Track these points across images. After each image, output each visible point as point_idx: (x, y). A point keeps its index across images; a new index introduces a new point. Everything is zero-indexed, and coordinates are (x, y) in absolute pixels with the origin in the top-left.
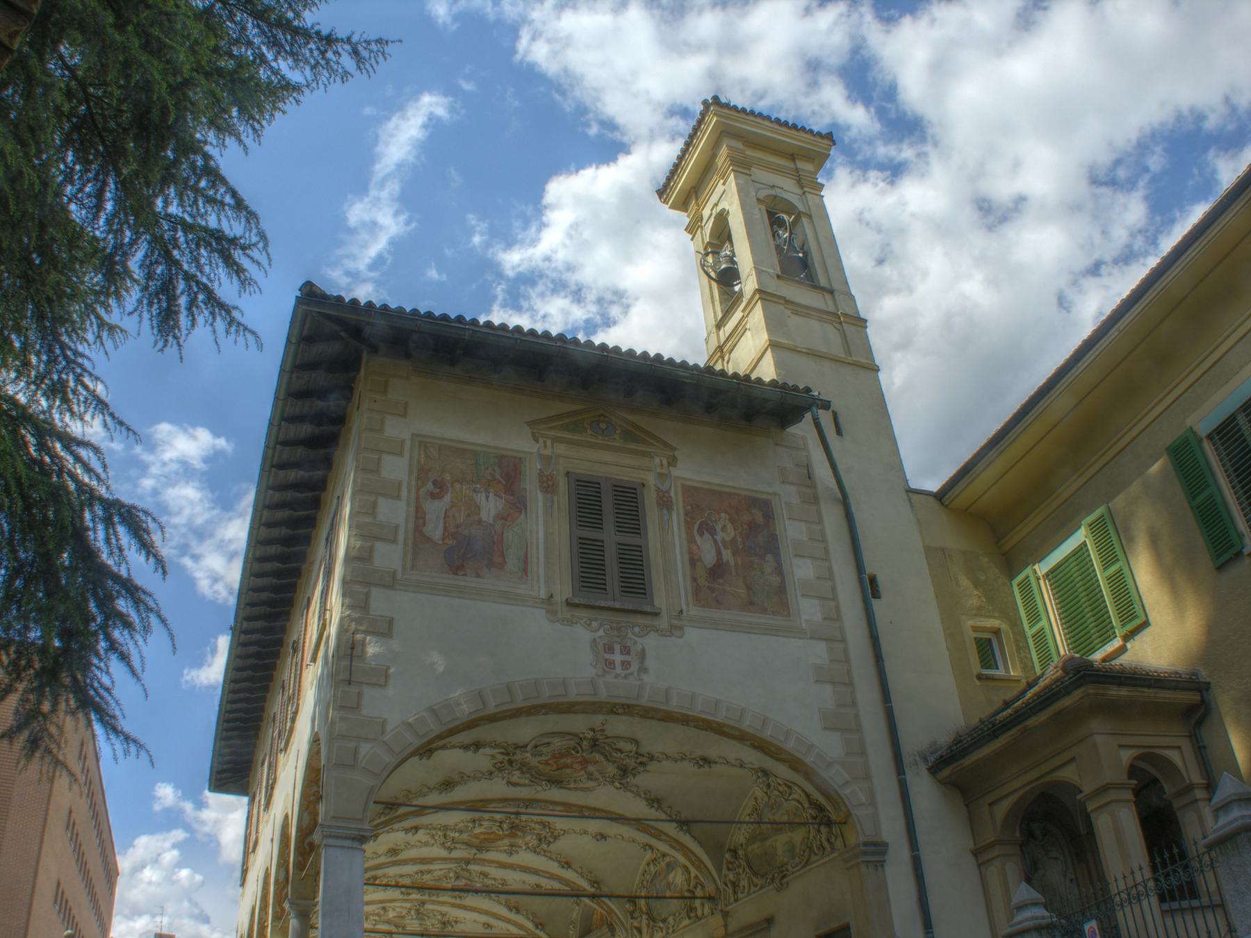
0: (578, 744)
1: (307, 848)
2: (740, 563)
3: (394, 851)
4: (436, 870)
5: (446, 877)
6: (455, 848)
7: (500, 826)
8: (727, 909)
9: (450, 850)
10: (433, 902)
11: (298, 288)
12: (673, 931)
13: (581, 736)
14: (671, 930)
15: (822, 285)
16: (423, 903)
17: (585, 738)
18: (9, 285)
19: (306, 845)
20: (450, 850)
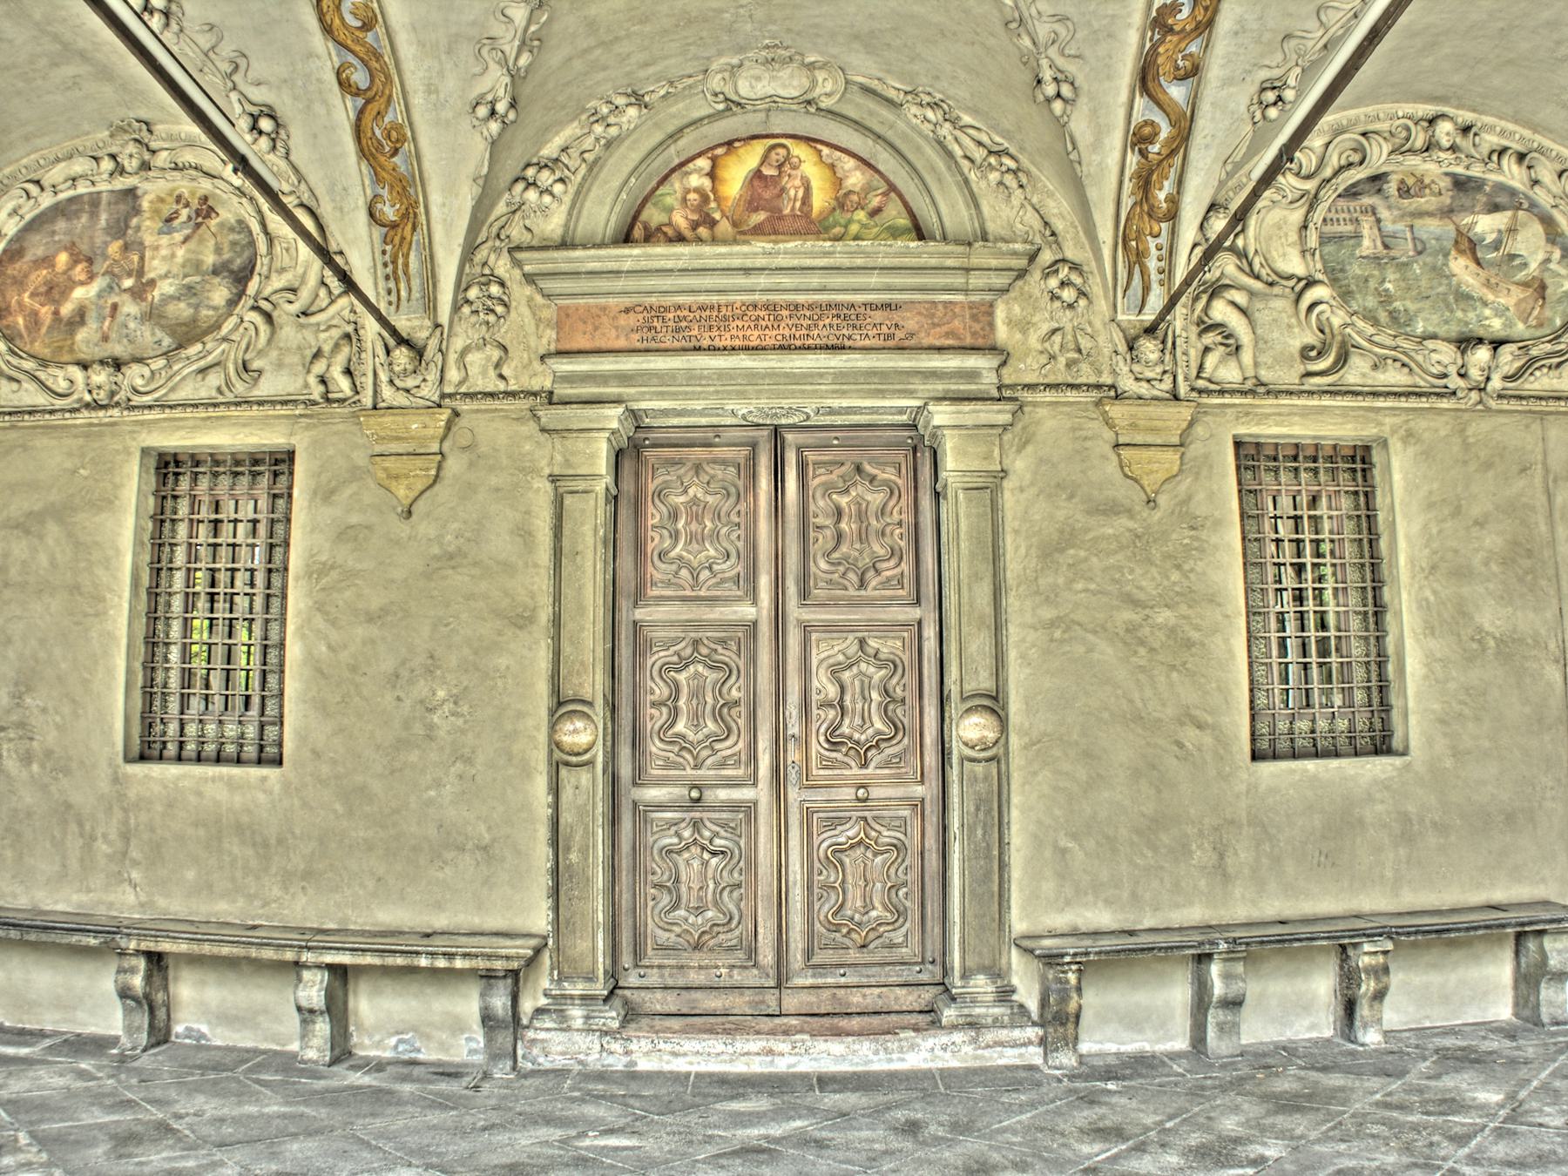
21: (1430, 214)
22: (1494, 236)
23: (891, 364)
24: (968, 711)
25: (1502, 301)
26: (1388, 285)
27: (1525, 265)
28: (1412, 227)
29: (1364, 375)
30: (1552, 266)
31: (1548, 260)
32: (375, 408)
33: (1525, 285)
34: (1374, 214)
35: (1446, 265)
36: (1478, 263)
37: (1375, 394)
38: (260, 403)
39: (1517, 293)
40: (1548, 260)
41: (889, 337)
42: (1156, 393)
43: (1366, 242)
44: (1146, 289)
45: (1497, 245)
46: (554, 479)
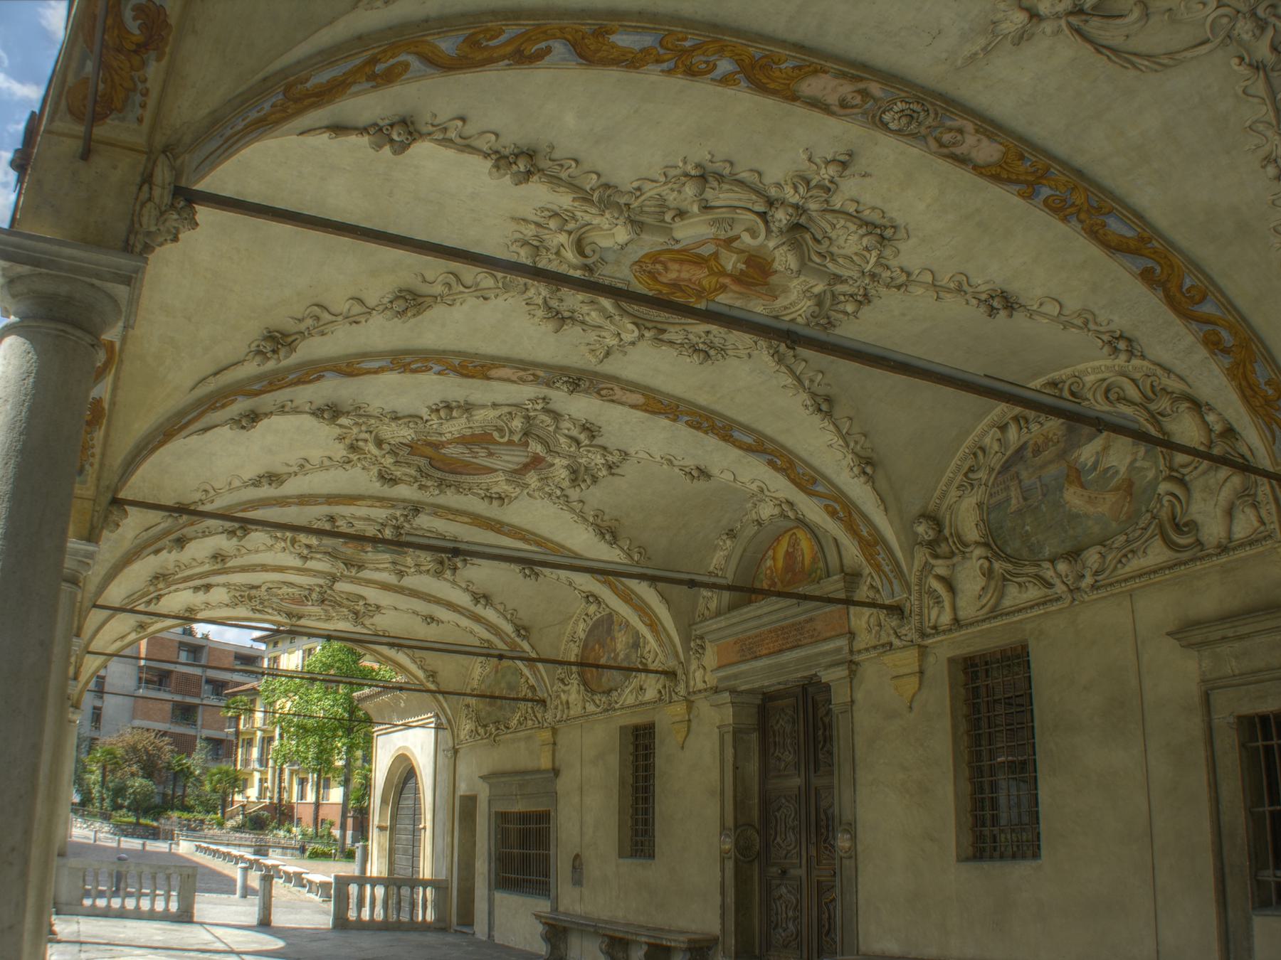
0: (379, 531)
1: (133, 26)
2: (1073, 498)
3: (218, 557)
4: (483, 406)
5: (500, 430)
6: (311, 558)
7: (763, 215)
8: (692, 699)
9: (305, 558)
10: (439, 511)
11: (1034, 863)
12: (1094, 587)
13: (773, 192)
14: (1088, 580)
15: (1265, 480)
16: (334, 579)
17: (783, 203)
18: (99, 792)
19: (128, 14)
20: (305, 558)
21: (1051, 462)
22: (1093, 459)
23: (803, 654)
24: (470, 137)
25: (1100, 510)
26: (1028, 528)
27: (1117, 472)
28: (1040, 477)
29: (1014, 598)
30: (1138, 464)
31: (1135, 460)
32: (1238, 12)
33: (1117, 489)
34: (1018, 477)
35: (1062, 497)
36: (1083, 486)
37: (1020, 611)
38: (1126, 580)
39: (1111, 498)
40: (1135, 460)
41: (812, 636)
42: (904, 643)
43: (1014, 501)
44: (891, 583)
45: (1094, 467)
46: (718, 727)
